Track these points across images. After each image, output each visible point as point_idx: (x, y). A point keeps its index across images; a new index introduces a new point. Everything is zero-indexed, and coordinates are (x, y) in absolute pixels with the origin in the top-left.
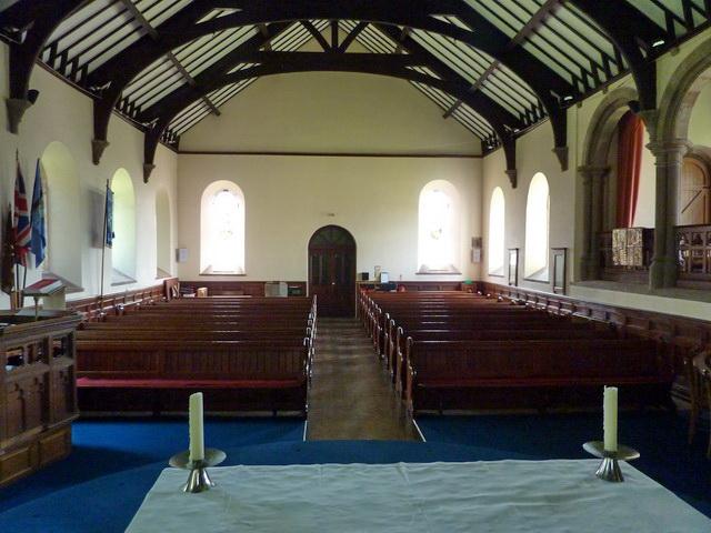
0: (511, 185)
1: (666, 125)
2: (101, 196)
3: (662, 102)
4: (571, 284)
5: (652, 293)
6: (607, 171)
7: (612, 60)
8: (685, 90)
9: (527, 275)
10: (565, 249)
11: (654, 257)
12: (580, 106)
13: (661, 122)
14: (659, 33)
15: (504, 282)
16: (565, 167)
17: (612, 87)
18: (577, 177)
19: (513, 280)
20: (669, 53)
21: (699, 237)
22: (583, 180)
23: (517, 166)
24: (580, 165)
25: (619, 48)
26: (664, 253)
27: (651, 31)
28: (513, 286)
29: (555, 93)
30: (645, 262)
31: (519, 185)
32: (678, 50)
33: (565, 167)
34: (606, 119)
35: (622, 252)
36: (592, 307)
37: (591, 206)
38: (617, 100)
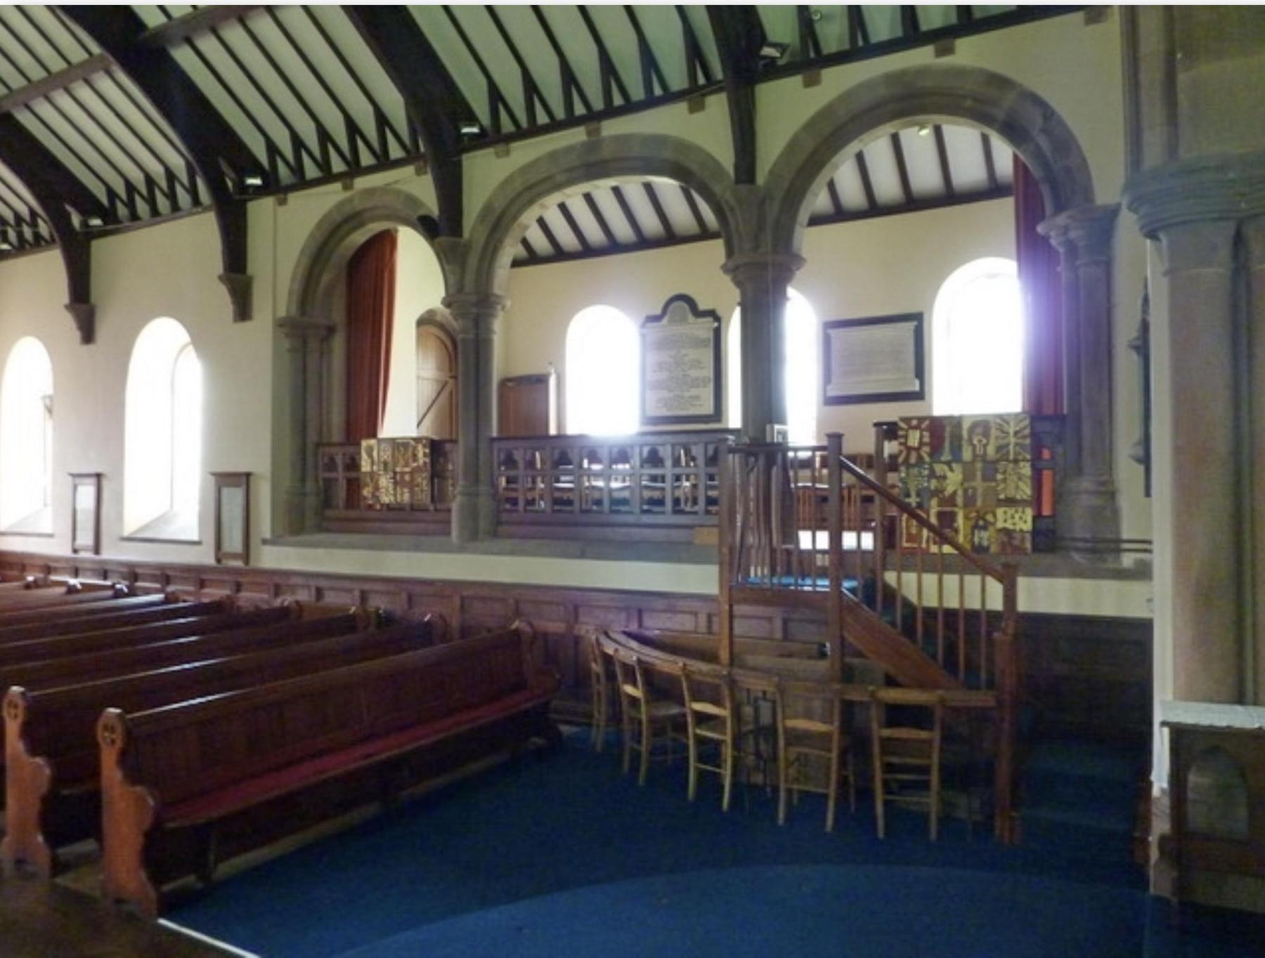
0: (76, 335)
1: (479, 271)
2: (633, 667)
3: (473, 229)
4: (265, 542)
5: (461, 549)
6: (331, 330)
7: (122, 201)
8: (515, 218)
9: (129, 528)
10: (99, 476)
11: (459, 489)
12: (283, 202)
13: (473, 260)
14: (257, 169)
15: (58, 548)
16: (243, 311)
17: (362, 183)
18: (275, 339)
19: (85, 538)
20: (490, 151)
21: (332, 460)
22: (287, 344)
23: (95, 296)
24: (282, 313)
25: (197, 169)
26: (477, 481)
27: (247, 164)
28: (88, 555)
29: (226, 170)
30: (438, 496)
31: (104, 329)
32: (507, 153)
33: (243, 311)
34: (342, 239)
35: (385, 481)
36: (323, 583)
37: (1249, 329)
38: (373, 208)
